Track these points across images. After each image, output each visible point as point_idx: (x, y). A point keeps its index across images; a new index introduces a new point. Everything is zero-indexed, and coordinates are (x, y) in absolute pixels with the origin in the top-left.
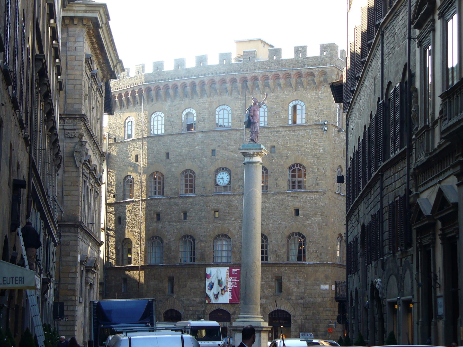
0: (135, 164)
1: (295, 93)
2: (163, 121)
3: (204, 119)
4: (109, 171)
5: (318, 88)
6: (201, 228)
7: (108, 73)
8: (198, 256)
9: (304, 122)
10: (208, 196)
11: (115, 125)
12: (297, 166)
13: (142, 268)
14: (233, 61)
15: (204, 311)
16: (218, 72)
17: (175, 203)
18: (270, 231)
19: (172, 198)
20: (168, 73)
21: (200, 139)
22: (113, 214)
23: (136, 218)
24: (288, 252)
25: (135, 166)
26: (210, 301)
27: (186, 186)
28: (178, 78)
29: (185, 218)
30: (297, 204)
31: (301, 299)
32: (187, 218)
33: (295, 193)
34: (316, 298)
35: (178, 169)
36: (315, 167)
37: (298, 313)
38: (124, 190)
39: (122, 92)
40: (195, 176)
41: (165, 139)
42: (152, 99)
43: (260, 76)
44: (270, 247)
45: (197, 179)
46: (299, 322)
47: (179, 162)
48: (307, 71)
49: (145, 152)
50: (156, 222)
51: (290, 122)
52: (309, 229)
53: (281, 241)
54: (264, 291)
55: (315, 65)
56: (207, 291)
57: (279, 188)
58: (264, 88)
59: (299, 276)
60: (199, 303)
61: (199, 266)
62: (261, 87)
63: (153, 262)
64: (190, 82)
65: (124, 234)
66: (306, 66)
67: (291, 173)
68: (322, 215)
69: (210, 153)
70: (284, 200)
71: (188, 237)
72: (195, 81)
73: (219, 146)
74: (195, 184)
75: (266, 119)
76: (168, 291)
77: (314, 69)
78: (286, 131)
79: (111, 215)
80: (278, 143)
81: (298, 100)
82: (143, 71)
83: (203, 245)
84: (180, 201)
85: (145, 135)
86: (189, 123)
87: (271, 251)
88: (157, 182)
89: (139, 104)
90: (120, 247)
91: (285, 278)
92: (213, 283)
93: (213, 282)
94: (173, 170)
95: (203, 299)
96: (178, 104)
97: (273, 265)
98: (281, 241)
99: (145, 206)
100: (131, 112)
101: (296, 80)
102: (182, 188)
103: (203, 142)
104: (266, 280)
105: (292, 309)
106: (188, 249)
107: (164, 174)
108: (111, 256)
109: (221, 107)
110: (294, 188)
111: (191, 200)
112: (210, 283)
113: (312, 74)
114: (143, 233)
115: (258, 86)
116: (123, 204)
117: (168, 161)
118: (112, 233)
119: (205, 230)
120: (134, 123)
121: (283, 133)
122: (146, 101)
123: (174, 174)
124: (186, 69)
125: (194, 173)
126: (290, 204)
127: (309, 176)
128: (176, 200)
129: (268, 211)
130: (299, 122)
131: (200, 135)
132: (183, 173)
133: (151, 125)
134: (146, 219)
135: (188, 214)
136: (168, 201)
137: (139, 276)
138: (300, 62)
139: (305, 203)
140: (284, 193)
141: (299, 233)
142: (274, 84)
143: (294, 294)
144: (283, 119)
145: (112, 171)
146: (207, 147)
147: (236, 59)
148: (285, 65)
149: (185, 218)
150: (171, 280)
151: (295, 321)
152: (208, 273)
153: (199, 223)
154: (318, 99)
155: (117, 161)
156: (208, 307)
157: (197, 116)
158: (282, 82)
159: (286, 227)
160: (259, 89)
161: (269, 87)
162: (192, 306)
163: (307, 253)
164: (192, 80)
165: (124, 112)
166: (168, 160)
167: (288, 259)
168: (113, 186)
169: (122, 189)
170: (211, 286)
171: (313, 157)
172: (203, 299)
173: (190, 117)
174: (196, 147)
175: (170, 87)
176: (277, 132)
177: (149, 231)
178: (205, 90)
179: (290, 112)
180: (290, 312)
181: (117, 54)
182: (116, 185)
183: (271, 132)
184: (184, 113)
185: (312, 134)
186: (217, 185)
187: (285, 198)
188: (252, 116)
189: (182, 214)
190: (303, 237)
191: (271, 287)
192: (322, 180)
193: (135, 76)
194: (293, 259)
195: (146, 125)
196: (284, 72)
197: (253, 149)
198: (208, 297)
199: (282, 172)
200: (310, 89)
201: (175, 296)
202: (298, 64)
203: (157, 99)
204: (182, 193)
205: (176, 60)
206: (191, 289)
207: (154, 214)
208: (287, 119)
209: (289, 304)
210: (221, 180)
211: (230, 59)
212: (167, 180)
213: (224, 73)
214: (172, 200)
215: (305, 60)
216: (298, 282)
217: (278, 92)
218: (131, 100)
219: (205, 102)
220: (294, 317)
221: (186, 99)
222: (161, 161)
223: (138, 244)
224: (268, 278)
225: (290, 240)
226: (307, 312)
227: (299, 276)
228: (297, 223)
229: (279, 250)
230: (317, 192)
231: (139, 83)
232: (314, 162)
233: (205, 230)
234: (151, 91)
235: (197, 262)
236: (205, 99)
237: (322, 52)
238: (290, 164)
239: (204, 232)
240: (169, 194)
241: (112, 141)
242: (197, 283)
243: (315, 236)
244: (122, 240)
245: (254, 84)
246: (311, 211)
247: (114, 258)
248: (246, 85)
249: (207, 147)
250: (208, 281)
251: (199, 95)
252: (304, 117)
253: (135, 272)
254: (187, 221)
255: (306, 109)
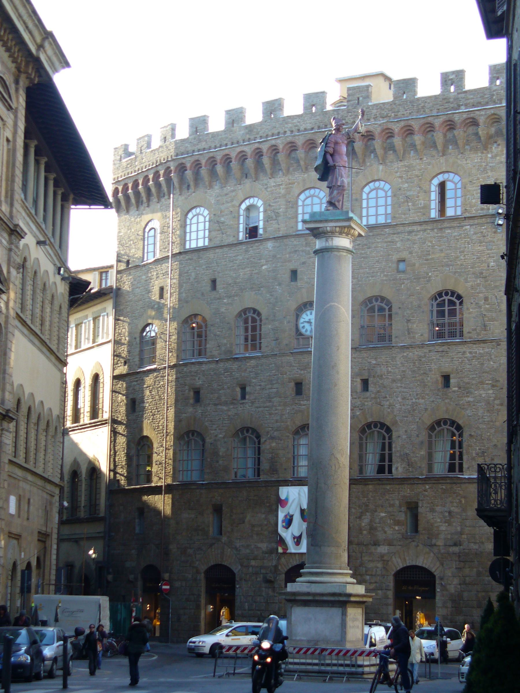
0: (159, 303)
1: (442, 160)
2: (207, 224)
3: (277, 215)
4: (118, 320)
5: (485, 148)
6: (270, 414)
7: (27, 65)
8: (265, 465)
9: (459, 213)
10: (284, 355)
11: (129, 237)
12: (447, 294)
13: (169, 489)
14: (329, 108)
15: (276, 567)
16: (302, 128)
17: (226, 370)
18: (397, 418)
19: (221, 360)
20: (214, 135)
21: (270, 251)
22: (123, 395)
23: (160, 399)
24: (430, 456)
25: (159, 306)
26: (286, 548)
27: (246, 339)
28: (232, 144)
29: (243, 397)
30: (447, 366)
31: (455, 545)
32: (247, 397)
33: (443, 344)
34: (483, 543)
35: (231, 309)
36: (481, 295)
37: (449, 573)
38: (141, 351)
39: (139, 176)
40: (261, 320)
41: (210, 255)
42: (189, 186)
43: (377, 131)
44: (396, 447)
45: (265, 324)
46: (452, 589)
47: (234, 296)
48: (465, 116)
49: (174, 281)
50: (193, 405)
51: (434, 214)
52: (469, 412)
53: (418, 436)
54: (386, 529)
55: (479, 104)
56: (281, 530)
57: (414, 337)
58: (386, 153)
59: (452, 502)
60: (266, 553)
61: (268, 484)
62: (380, 151)
63: (186, 477)
64: (252, 149)
65: (141, 429)
66: (463, 107)
67: (435, 309)
68: (493, 386)
69: (287, 276)
70: (423, 359)
71: (248, 431)
72: (260, 146)
73: (304, 263)
74: (260, 334)
75: (389, 211)
76: (212, 531)
77: (477, 113)
78: (425, 230)
79: (120, 395)
80: (411, 253)
81: (448, 172)
82: (173, 136)
83: (274, 444)
84: (235, 366)
85: (176, 251)
86: (251, 225)
87: (398, 454)
88: (195, 331)
89: (166, 197)
90: (133, 452)
91: (425, 505)
92: (292, 516)
93: (291, 513)
94: (223, 310)
95: (274, 545)
96: (233, 191)
97: (403, 481)
98: (418, 436)
99: (174, 377)
100: (153, 212)
101: (445, 135)
102: (238, 343)
103: (274, 256)
104: (390, 509)
105: (438, 564)
106: (250, 453)
107: (207, 317)
108: (119, 471)
109: (307, 192)
110: (440, 335)
111: (253, 362)
112: (286, 516)
113: (474, 122)
114: (171, 426)
115: (374, 151)
116: (138, 376)
117: (214, 294)
118: (121, 429)
119: (278, 418)
120: (158, 231)
121: (421, 235)
122: (178, 190)
123: (224, 318)
124: (247, 127)
125: (259, 314)
126: (433, 366)
127: (470, 313)
128: (228, 365)
129: (394, 381)
130: (450, 212)
131: (270, 245)
132: (239, 315)
133: (185, 233)
134: (177, 401)
135: (248, 389)
136: (213, 366)
137: (162, 503)
138: (451, 100)
139: (461, 363)
140: (422, 346)
141: (449, 419)
142: (403, 145)
143: (442, 536)
144: (420, 208)
145: (122, 318)
146: (282, 266)
147: (334, 104)
148: (423, 107)
149: (243, 397)
150: (218, 510)
151: (444, 588)
152: (283, 497)
153: (268, 404)
154: (485, 169)
155: (131, 301)
156: (283, 560)
157: (265, 211)
158: (418, 139)
159: (426, 409)
160: (376, 156)
161: (395, 151)
162: (255, 558)
163: (465, 457)
164: (257, 145)
165: (142, 214)
166: (214, 293)
167: (430, 468)
168: (124, 344)
169: (138, 350)
170: (289, 522)
171: (477, 277)
172: (274, 545)
173: (253, 214)
174: (264, 268)
175: (219, 161)
176: (410, 232)
177: (180, 421)
178: (279, 163)
179: (434, 196)
180: (433, 570)
181: (34, 12)
182: (129, 342)
183: (398, 233)
184: (243, 206)
185: (475, 233)
186: (301, 334)
187: (425, 356)
188: (332, 155)
189: (238, 390)
190: (459, 428)
191: (398, 523)
192: (493, 320)
193: (160, 147)
194: (440, 468)
195: (178, 232)
196: (422, 121)
197: (331, 221)
198: (282, 541)
199: (419, 307)
200: (471, 150)
201: (224, 539)
202: (447, 105)
203: (196, 185)
204: (238, 352)
205: (228, 112)
206: (253, 526)
207: (189, 391)
208: (427, 208)
209: (432, 554)
210: (307, 326)
211: (324, 104)
212: (212, 328)
213: (312, 129)
214: (221, 365)
215: (460, 96)
216: (450, 513)
217: (412, 159)
218: (153, 190)
219: (279, 185)
220: (441, 579)
221: (246, 180)
222: (203, 294)
223: (162, 446)
224: (392, 505)
225: (433, 435)
226: (467, 571)
227: (452, 502)
228: (446, 401)
229: (413, 453)
230: (484, 341)
231: (166, 157)
232: (478, 285)
233: (278, 418)
234: (186, 170)
235: (263, 478)
236: (280, 179)
237: (492, 80)
238: (433, 291)
239: (277, 421)
240: (215, 353)
241: (123, 266)
242: (263, 516)
243: (481, 426)
244: (137, 440)
245: (367, 147)
246: (473, 379)
247: (125, 472)
248: (353, 149)
249: (282, 266)
250: (282, 512)
251: (269, 171)
252: (459, 203)
253: (157, 496)
254: (246, 401)
255: (464, 187)
